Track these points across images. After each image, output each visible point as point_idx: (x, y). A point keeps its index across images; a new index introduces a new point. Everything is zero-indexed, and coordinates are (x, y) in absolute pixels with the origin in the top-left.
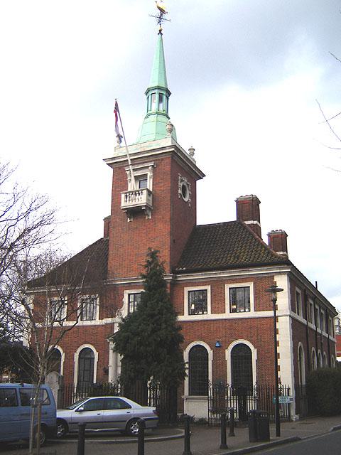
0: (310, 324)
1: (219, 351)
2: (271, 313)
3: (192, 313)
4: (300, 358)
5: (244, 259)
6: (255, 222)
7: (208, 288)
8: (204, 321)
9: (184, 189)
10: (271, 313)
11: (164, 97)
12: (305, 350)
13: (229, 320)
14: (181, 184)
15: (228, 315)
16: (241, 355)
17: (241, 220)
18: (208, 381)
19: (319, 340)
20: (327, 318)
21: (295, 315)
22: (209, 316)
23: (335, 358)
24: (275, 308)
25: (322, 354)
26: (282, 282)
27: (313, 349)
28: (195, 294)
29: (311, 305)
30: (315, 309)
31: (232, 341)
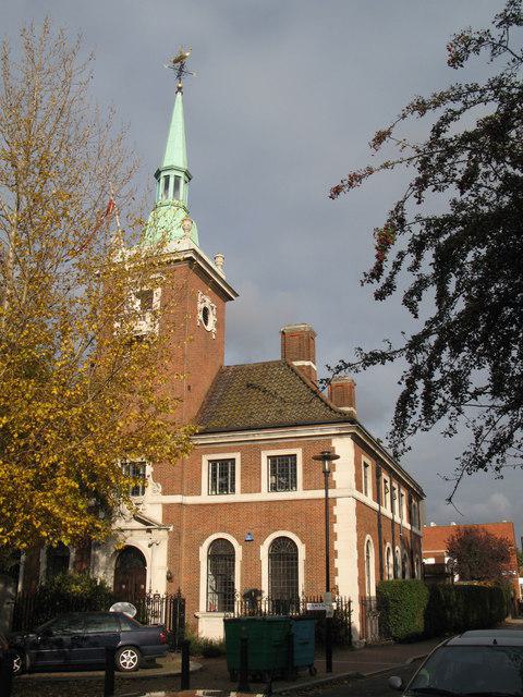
0: (383, 510)
1: (251, 544)
2: (321, 494)
3: (274, 488)
4: (368, 557)
5: (257, 419)
6: (307, 363)
7: (237, 456)
8: (230, 504)
9: (205, 311)
10: (321, 494)
11: (182, 182)
12: (375, 545)
13: (266, 502)
14: (201, 306)
15: (265, 495)
16: (283, 554)
17: (288, 360)
18: (233, 590)
19: (396, 533)
20: (410, 502)
21: (362, 497)
22: (238, 497)
23: (421, 560)
24: (328, 484)
25: (394, 548)
26: (344, 448)
27: (389, 545)
28: (275, 461)
29: (386, 482)
30: (393, 489)
31: (296, 533)
